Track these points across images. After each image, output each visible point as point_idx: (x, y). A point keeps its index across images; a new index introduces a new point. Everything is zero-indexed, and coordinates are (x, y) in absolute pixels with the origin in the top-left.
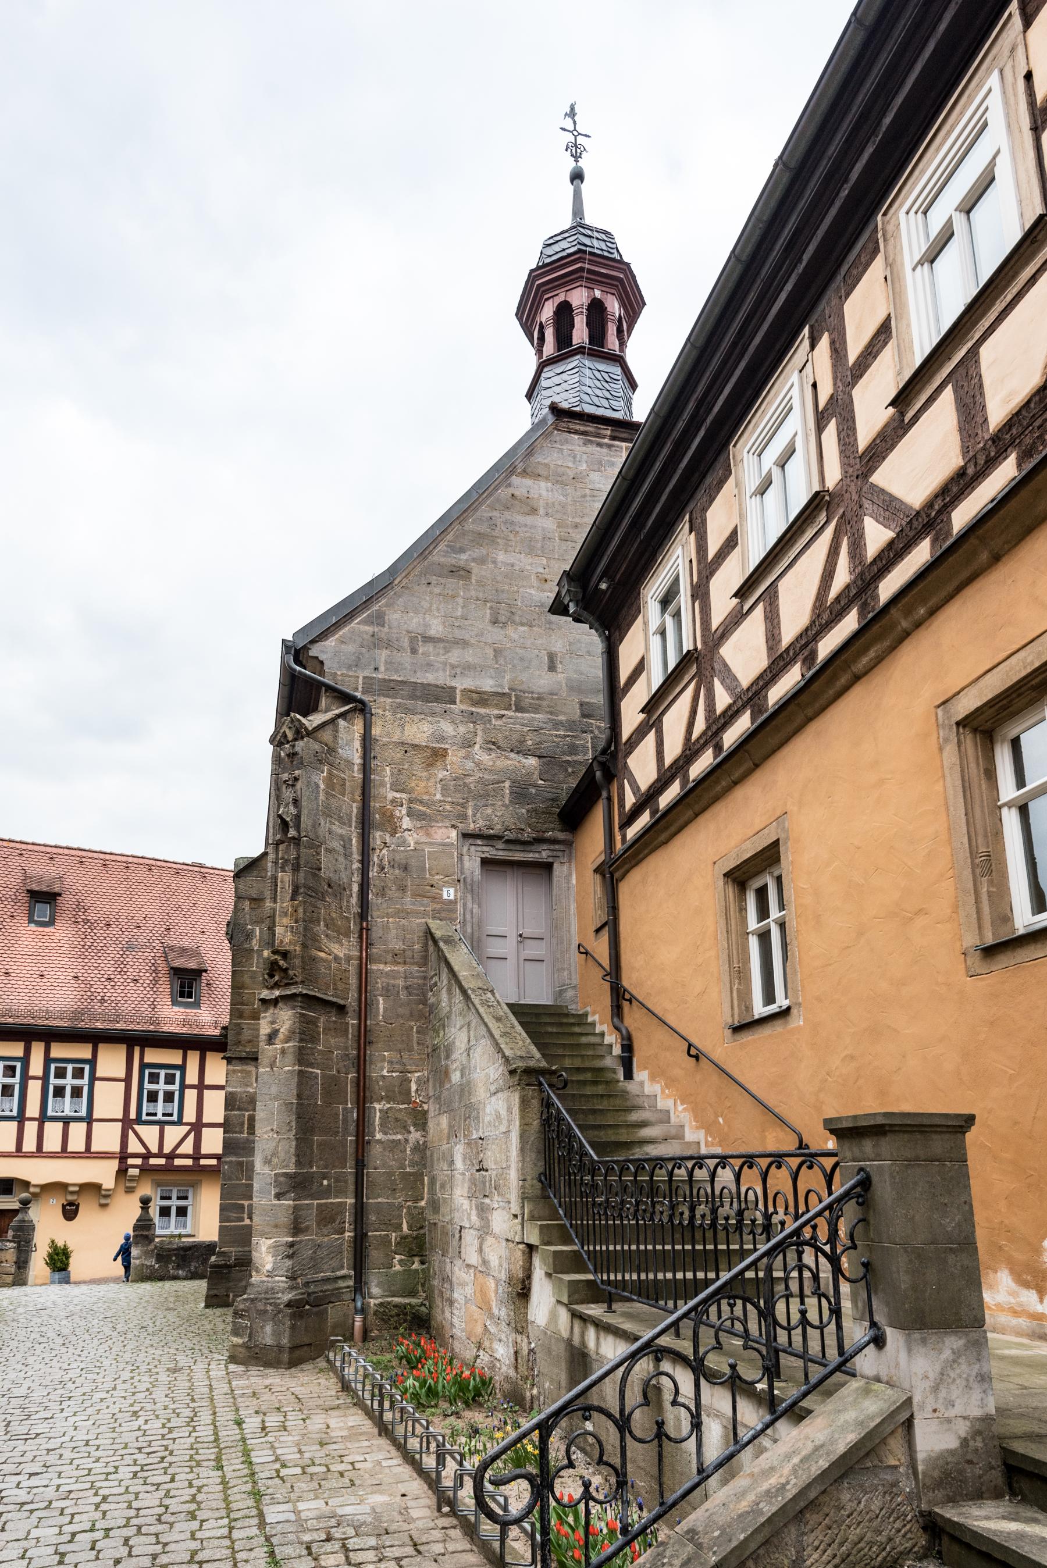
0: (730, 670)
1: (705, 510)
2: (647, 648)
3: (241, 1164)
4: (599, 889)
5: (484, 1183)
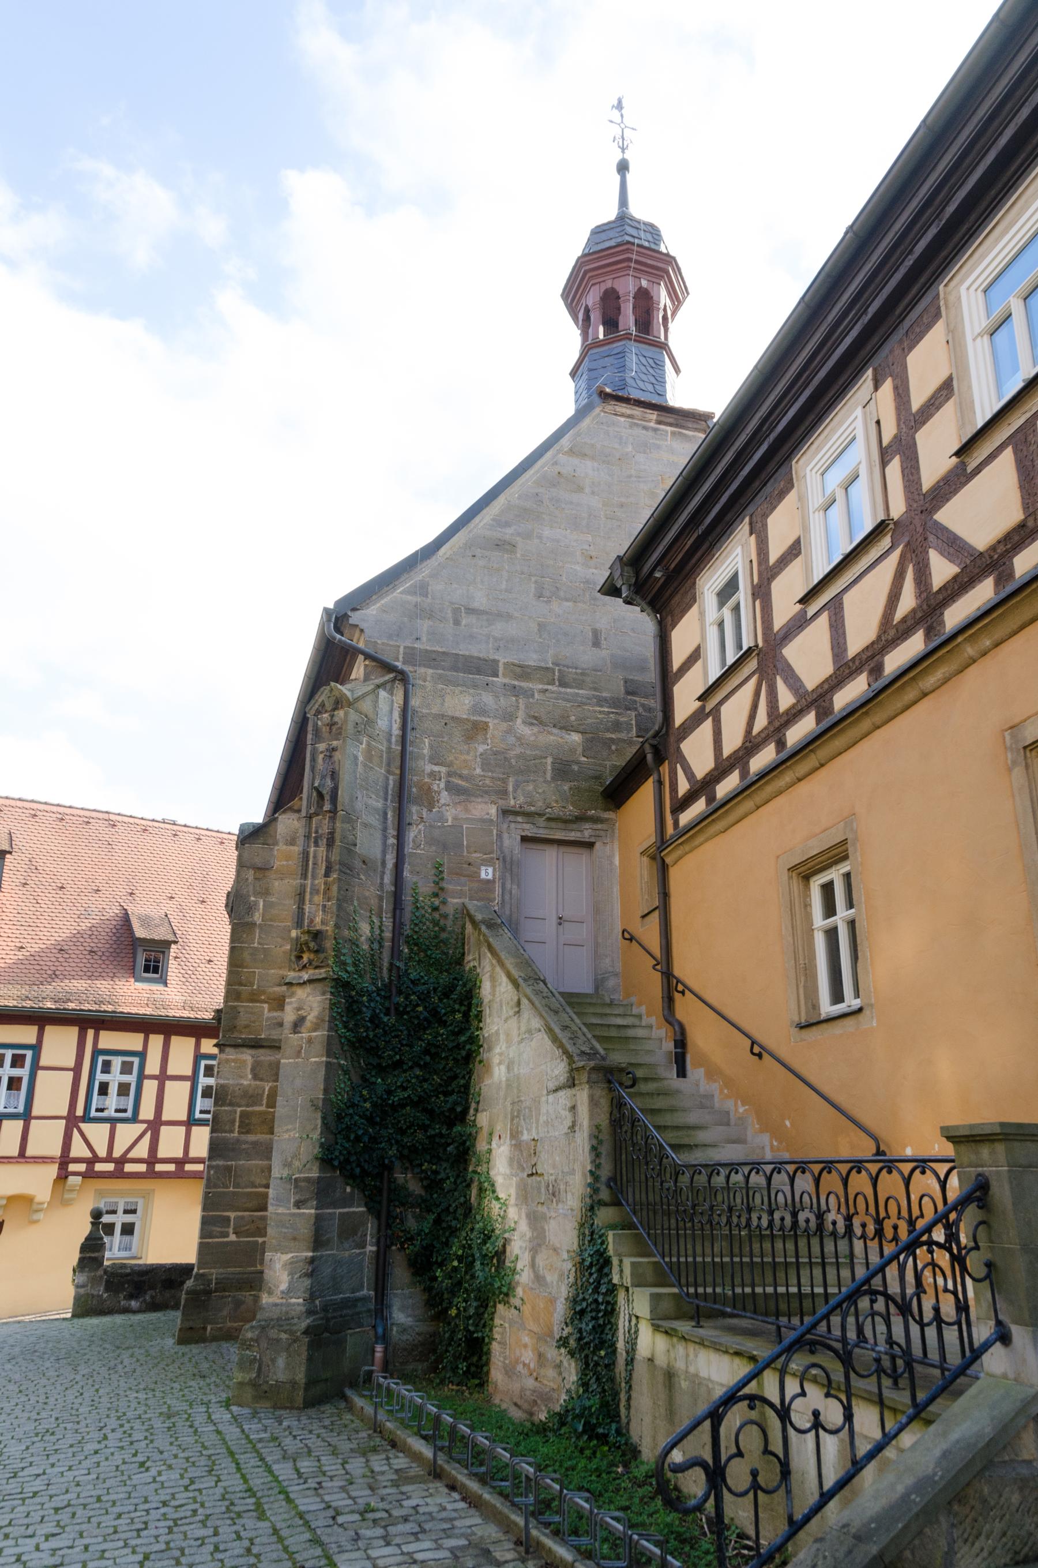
0: (792, 670)
1: (765, 516)
2: (703, 637)
3: (228, 1169)
4: (645, 873)
5: (539, 1189)
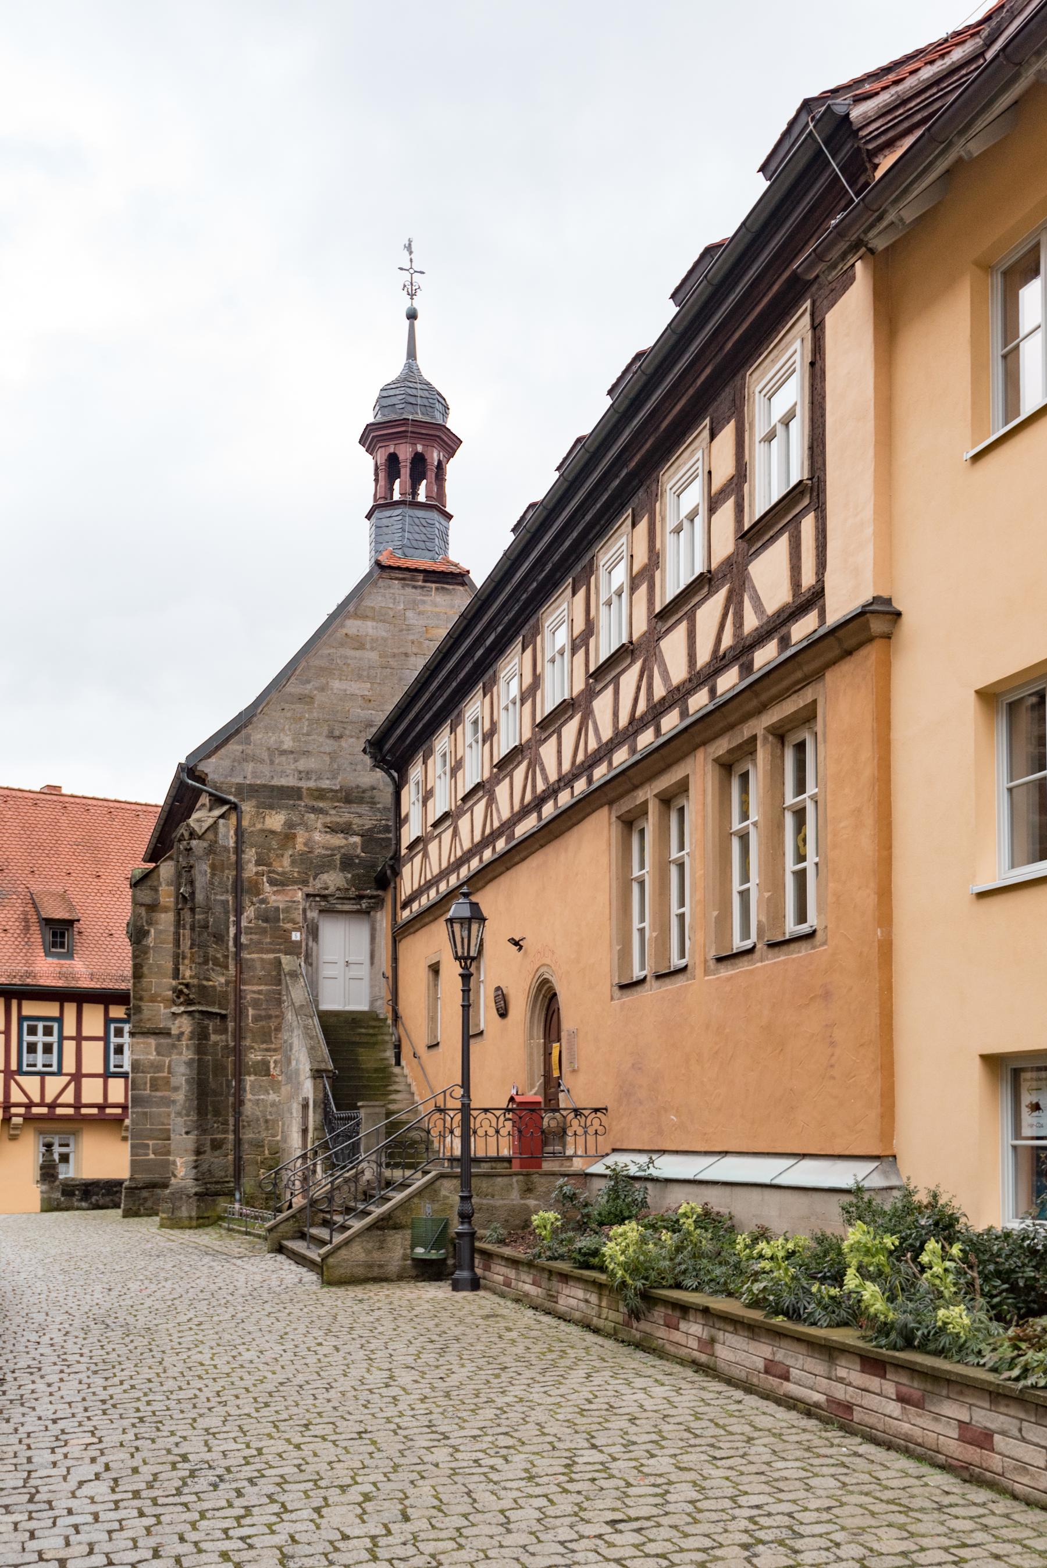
3: (145, 1113)
